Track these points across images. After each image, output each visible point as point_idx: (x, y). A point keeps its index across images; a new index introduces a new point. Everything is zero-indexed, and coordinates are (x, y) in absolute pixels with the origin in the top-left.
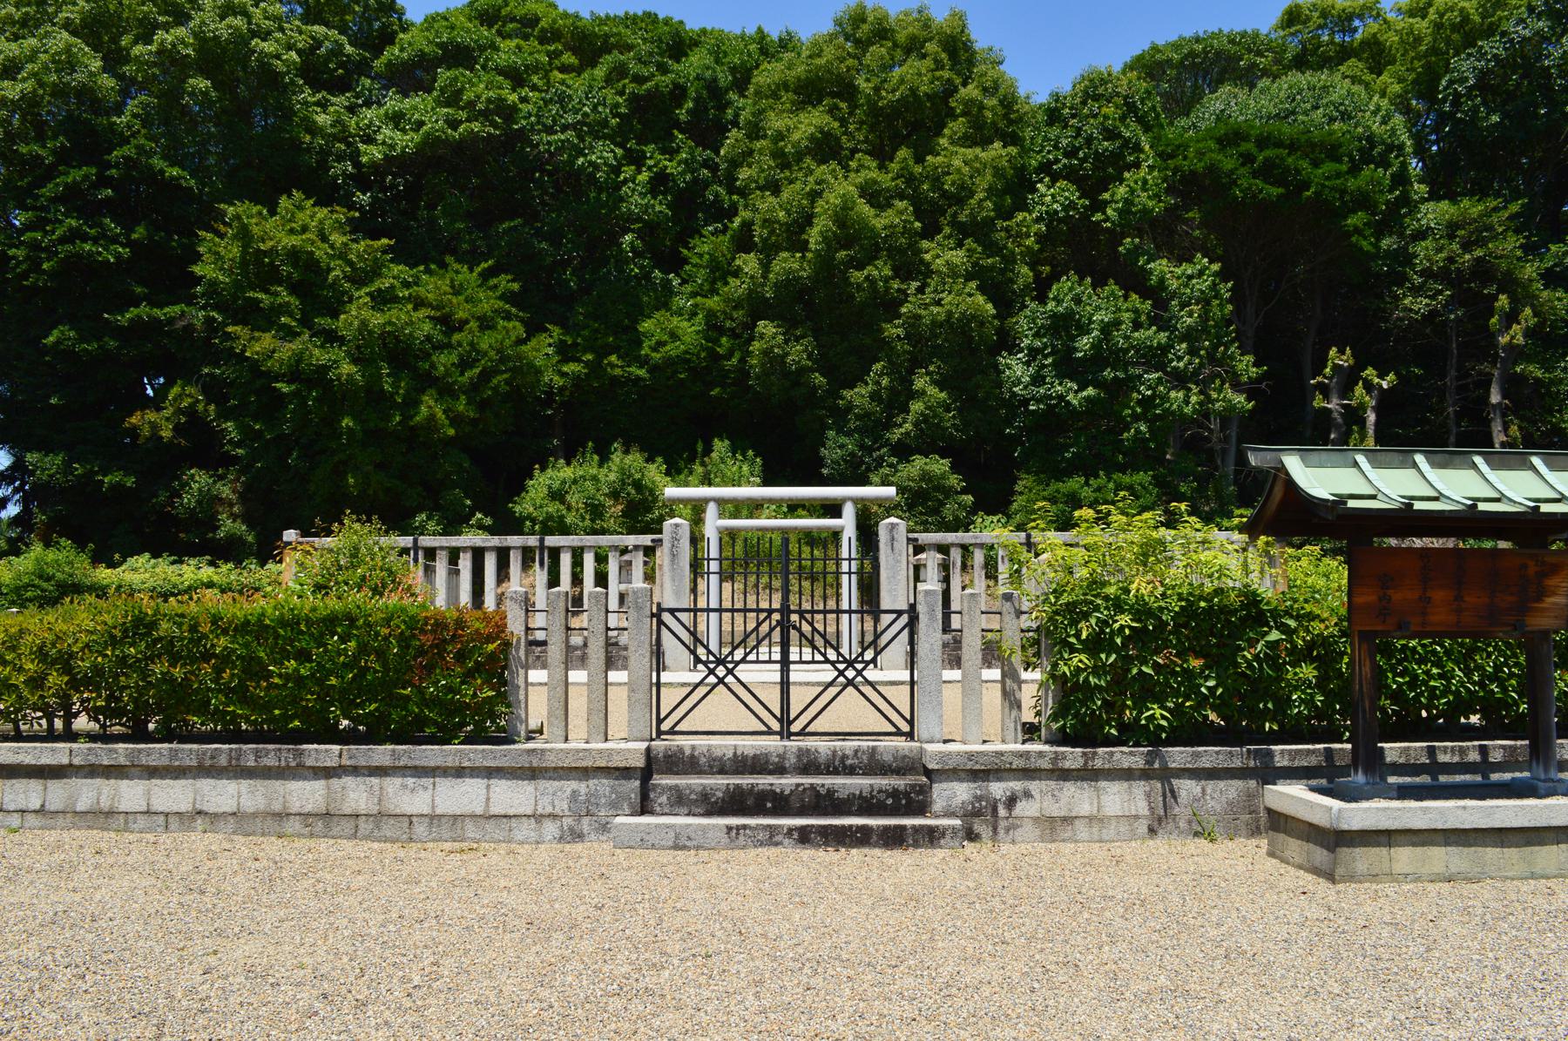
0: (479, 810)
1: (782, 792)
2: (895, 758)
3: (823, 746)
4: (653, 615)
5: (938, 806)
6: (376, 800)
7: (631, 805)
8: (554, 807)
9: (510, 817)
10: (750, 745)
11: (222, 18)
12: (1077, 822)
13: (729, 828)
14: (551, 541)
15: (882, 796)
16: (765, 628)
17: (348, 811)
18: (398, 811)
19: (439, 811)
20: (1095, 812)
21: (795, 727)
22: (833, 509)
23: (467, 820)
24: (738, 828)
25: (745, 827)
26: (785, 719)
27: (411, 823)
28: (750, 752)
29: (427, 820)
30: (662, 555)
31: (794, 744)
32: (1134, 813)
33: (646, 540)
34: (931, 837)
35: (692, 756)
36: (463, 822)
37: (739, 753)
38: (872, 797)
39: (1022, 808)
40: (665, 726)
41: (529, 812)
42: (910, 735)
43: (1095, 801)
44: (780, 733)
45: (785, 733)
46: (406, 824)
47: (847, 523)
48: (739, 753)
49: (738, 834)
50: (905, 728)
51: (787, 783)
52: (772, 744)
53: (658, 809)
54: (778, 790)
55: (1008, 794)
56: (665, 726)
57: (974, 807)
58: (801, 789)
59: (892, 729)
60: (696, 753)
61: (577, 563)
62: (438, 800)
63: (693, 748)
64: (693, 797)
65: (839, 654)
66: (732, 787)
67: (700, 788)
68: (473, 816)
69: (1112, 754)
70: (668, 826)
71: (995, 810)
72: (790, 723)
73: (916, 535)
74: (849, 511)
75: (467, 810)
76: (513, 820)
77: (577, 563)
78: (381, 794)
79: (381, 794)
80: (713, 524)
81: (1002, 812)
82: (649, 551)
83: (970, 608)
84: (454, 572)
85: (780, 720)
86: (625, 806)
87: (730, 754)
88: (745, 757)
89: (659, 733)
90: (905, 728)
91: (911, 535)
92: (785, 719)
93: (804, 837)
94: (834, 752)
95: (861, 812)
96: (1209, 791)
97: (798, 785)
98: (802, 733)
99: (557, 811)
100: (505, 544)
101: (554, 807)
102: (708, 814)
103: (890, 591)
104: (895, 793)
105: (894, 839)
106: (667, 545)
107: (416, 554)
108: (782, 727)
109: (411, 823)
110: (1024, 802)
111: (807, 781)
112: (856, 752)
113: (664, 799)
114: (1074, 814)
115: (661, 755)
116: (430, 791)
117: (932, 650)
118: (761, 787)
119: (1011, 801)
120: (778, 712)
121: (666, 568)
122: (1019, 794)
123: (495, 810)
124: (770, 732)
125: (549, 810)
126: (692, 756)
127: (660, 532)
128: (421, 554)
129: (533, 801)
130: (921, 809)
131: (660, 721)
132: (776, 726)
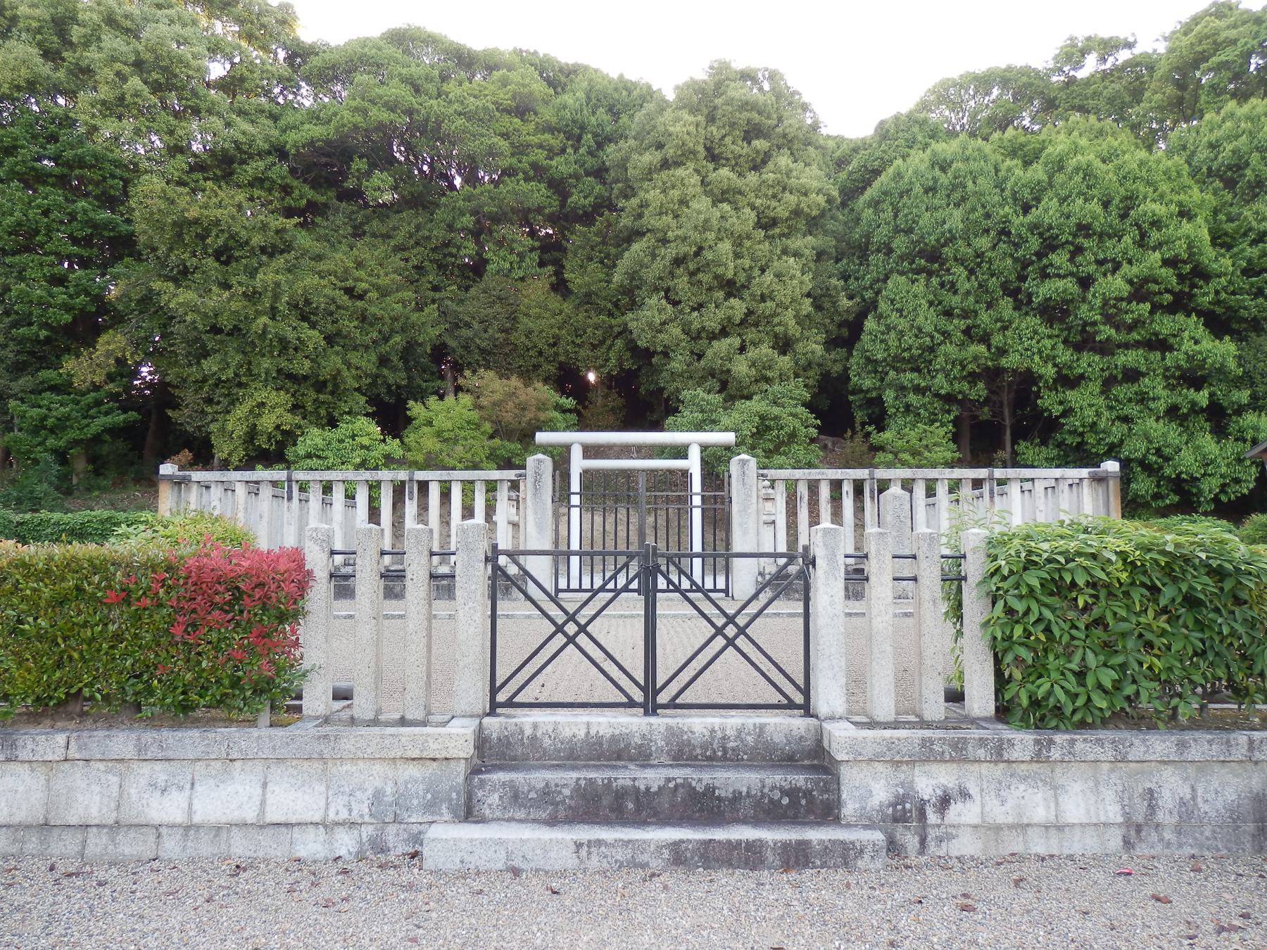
0: (250, 815)
1: (648, 789)
2: (789, 743)
3: (698, 724)
4: (487, 560)
5: (849, 809)
6: (113, 805)
7: (453, 811)
8: (350, 810)
9: (292, 825)
10: (606, 723)
11: (326, 205)
12: (1030, 831)
13: (579, 845)
14: (421, 475)
15: (776, 795)
16: (622, 580)
17: (73, 821)
18: (142, 820)
19: (197, 819)
20: (1052, 818)
21: (663, 698)
22: (680, 452)
23: (235, 829)
24: (589, 843)
25: (599, 843)
26: (650, 687)
27: (159, 836)
28: (605, 732)
29: (181, 831)
30: (526, 488)
31: (660, 722)
32: (1103, 819)
33: (511, 474)
34: (845, 855)
35: (534, 738)
36: (229, 831)
37: (593, 732)
38: (763, 795)
39: (956, 811)
40: (502, 697)
41: (317, 818)
42: (806, 709)
43: (1052, 805)
44: (644, 705)
45: (651, 707)
46: (152, 838)
47: (693, 464)
48: (593, 732)
49: (589, 853)
50: (799, 698)
51: (651, 778)
52: (632, 723)
53: (487, 812)
54: (642, 788)
55: (939, 792)
56: (502, 697)
57: (895, 810)
58: (671, 785)
59: (776, 698)
60: (539, 734)
61: (446, 495)
62: (197, 805)
63: (535, 726)
64: (532, 795)
65: (693, 583)
66: (583, 783)
67: (542, 785)
68: (244, 825)
69: (1072, 742)
70: (500, 842)
71: (922, 815)
72: (657, 692)
73: (765, 471)
74: (695, 454)
75: (236, 816)
76: (296, 829)
77: (446, 495)
78: (121, 796)
79: (121, 796)
80: (578, 464)
81: (932, 818)
82: (515, 486)
83: (878, 550)
84: (423, 508)
85: (644, 689)
86: (444, 811)
87: (582, 734)
88: (599, 741)
89: (494, 708)
90: (799, 698)
91: (761, 471)
92: (650, 687)
93: (678, 856)
94: (713, 731)
95: (756, 822)
96: (1200, 792)
97: (669, 780)
98: (673, 705)
99: (355, 816)
100: (376, 478)
101: (350, 810)
102: (552, 822)
103: (741, 525)
104: (792, 793)
105: (796, 857)
106: (530, 480)
107: (290, 487)
108: (646, 696)
109: (159, 836)
110: (960, 805)
111: (679, 774)
112: (739, 731)
113: (494, 799)
114: (1026, 821)
115: (494, 735)
116: (187, 792)
117: (832, 604)
118: (620, 782)
119: (944, 802)
120: (640, 676)
121: (529, 502)
122: (955, 793)
123: (273, 815)
124: (631, 704)
125: (344, 815)
126: (534, 738)
127: (524, 467)
128: (295, 488)
129: (323, 803)
130: (828, 813)
131: (494, 690)
132: (638, 696)
